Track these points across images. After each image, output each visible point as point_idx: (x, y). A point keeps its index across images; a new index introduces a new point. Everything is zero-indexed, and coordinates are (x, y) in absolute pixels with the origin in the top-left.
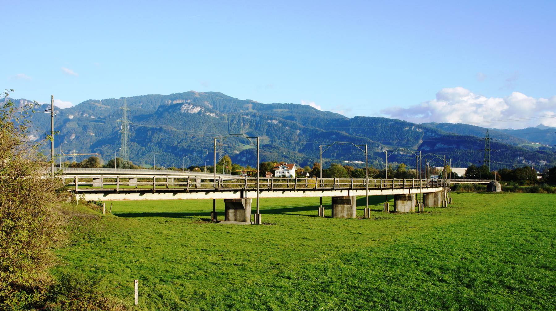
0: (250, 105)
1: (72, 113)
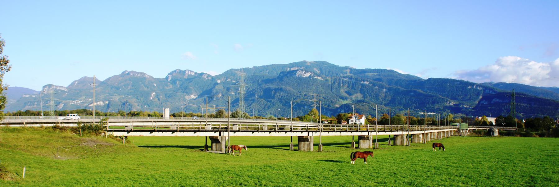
0: (348, 71)
1: (219, 79)
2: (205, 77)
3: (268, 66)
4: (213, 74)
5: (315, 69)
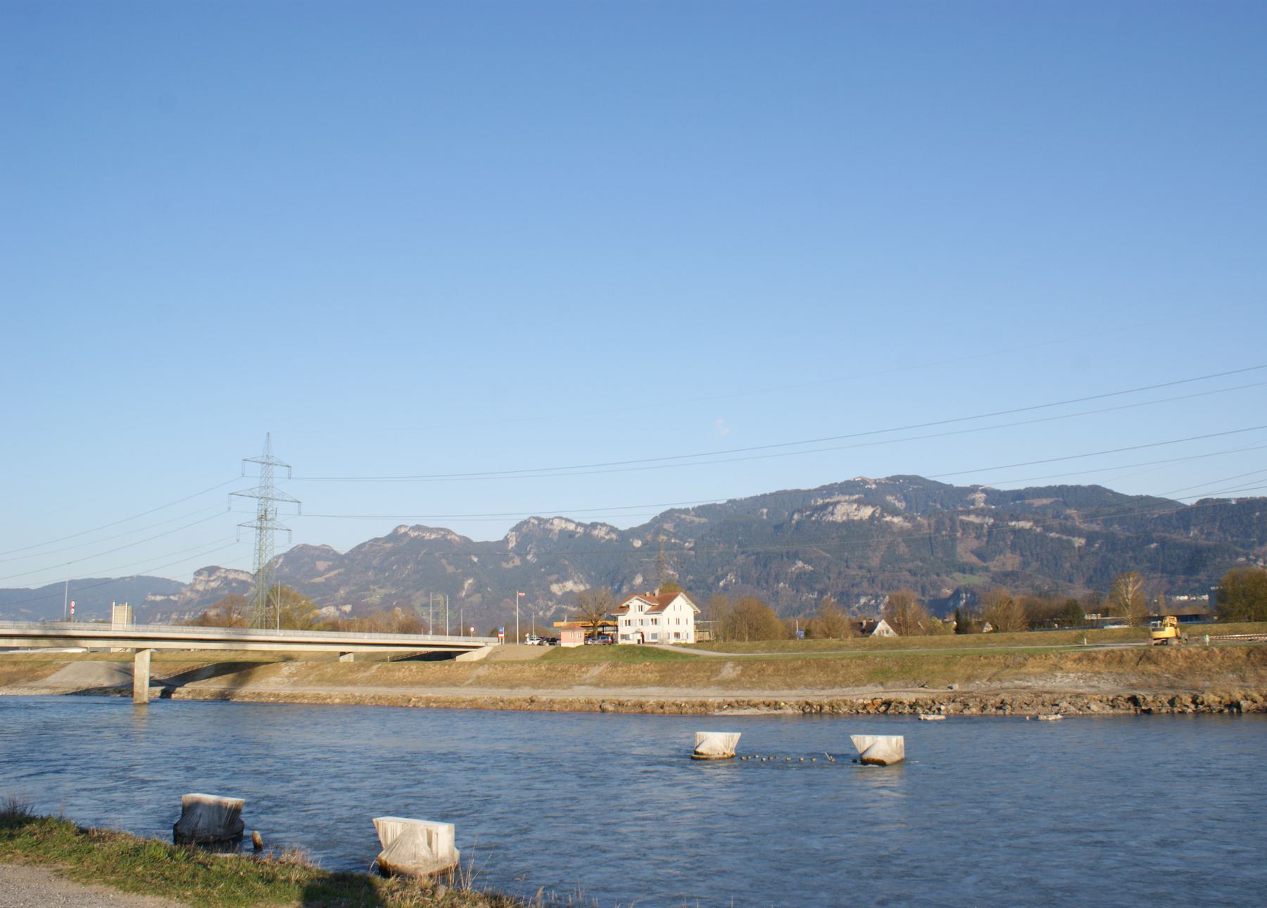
0: (980, 497)
1: (639, 537)
2: (602, 533)
3: (765, 496)
4: (623, 525)
5: (889, 498)
